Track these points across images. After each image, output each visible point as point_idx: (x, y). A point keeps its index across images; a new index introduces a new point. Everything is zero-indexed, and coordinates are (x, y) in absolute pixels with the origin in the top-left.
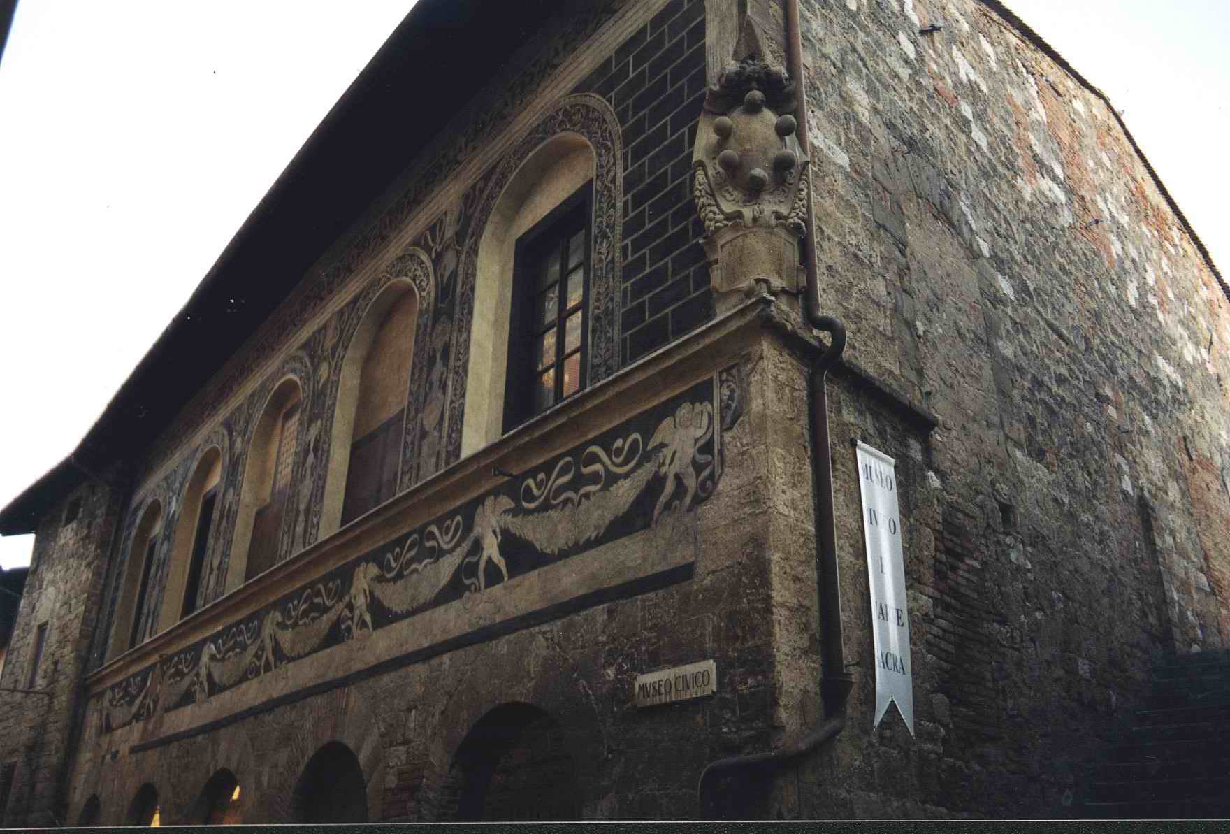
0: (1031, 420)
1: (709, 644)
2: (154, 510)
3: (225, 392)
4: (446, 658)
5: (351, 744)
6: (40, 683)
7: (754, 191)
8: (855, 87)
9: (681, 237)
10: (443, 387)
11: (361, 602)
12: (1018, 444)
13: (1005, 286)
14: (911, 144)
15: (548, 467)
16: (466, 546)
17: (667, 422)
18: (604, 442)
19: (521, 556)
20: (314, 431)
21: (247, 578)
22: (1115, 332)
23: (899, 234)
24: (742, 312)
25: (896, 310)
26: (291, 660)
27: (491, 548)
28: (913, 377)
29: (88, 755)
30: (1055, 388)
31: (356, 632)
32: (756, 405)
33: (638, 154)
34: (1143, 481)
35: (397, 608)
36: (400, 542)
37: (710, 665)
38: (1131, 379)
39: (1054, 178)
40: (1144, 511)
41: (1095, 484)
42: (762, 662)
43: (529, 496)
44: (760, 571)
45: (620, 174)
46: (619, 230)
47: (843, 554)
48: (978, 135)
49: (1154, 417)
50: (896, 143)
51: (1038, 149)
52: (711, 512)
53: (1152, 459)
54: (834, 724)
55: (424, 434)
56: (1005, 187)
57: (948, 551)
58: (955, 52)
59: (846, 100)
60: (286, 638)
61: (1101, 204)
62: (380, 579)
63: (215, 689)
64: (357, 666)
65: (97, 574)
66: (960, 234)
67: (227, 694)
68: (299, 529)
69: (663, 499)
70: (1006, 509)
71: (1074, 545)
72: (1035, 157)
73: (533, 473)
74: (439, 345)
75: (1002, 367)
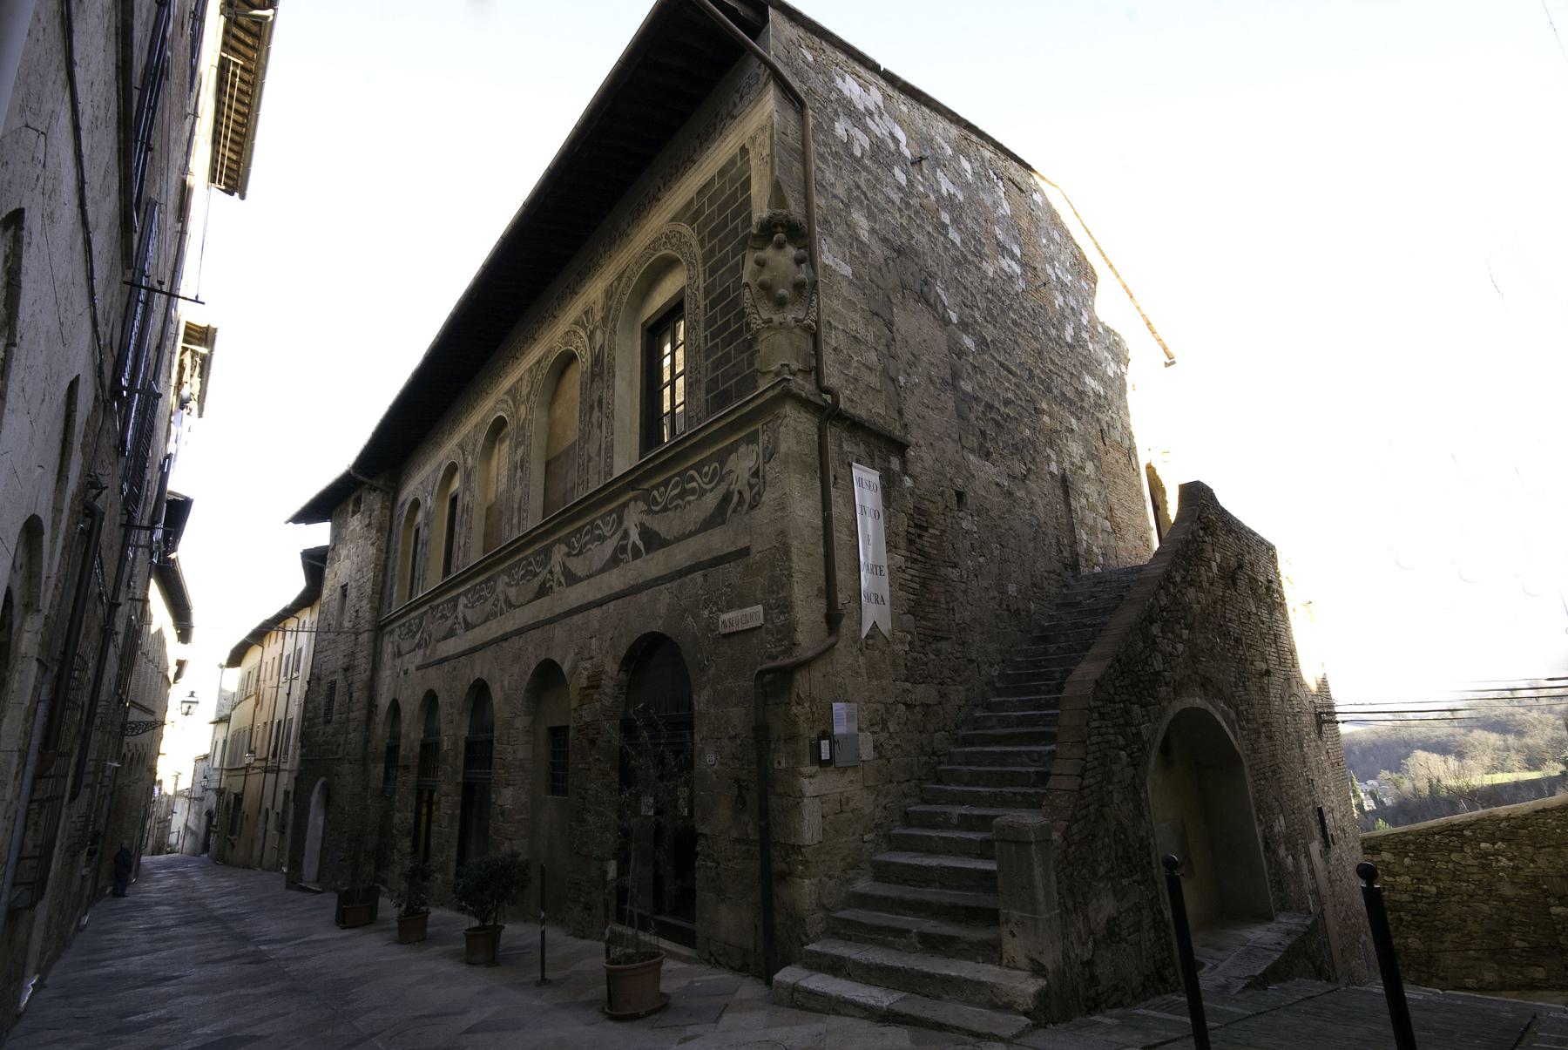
0: (983, 433)
1: (759, 595)
2: (416, 505)
3: (456, 422)
4: (611, 604)
5: (557, 660)
6: (347, 624)
7: (781, 303)
8: (859, 219)
9: (739, 332)
10: (600, 426)
11: (558, 569)
12: (972, 451)
13: (968, 342)
14: (899, 251)
15: (666, 483)
16: (619, 534)
17: (733, 456)
18: (698, 467)
19: (652, 540)
20: (520, 452)
21: (485, 552)
22: (1053, 362)
23: (888, 317)
24: (772, 387)
25: (885, 370)
26: (516, 607)
27: (634, 536)
28: (896, 415)
29: (388, 673)
30: (1002, 409)
31: (556, 588)
32: (783, 447)
33: (713, 271)
34: (1066, 465)
35: (580, 574)
36: (579, 530)
37: (760, 607)
38: (1063, 394)
39: (1013, 257)
40: (1065, 485)
41: (1029, 470)
42: (786, 606)
43: (655, 502)
44: (786, 550)
45: (702, 285)
46: (702, 325)
47: (840, 536)
48: (954, 235)
49: (1079, 419)
50: (888, 252)
51: (1000, 237)
52: (761, 515)
53: (1075, 449)
54: (832, 640)
55: (590, 459)
56: (972, 268)
57: (917, 526)
58: (939, 173)
59: (850, 226)
60: (512, 592)
61: (1049, 270)
62: (569, 555)
63: (468, 626)
64: (558, 610)
65: (379, 550)
66: (936, 310)
67: (477, 630)
68: (515, 521)
69: (732, 505)
70: (960, 496)
71: (1009, 511)
72: (999, 244)
73: (656, 487)
74: (596, 397)
75: (966, 401)
